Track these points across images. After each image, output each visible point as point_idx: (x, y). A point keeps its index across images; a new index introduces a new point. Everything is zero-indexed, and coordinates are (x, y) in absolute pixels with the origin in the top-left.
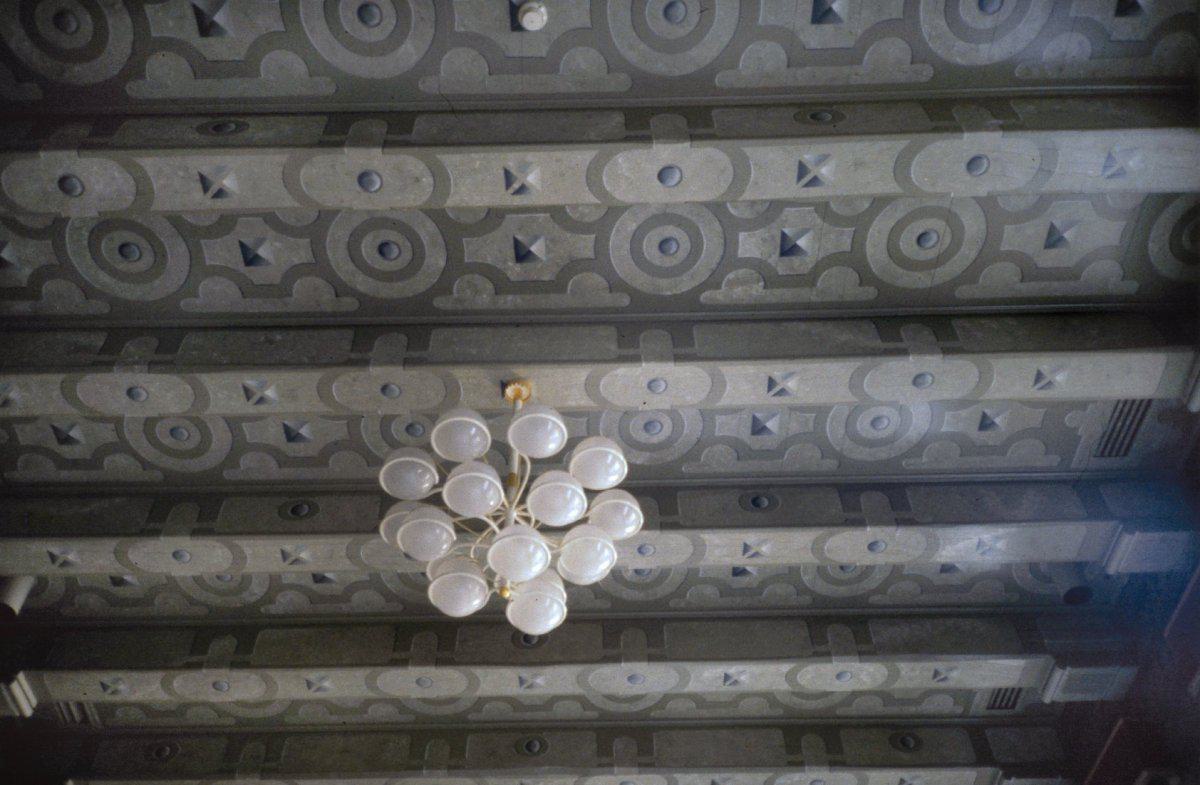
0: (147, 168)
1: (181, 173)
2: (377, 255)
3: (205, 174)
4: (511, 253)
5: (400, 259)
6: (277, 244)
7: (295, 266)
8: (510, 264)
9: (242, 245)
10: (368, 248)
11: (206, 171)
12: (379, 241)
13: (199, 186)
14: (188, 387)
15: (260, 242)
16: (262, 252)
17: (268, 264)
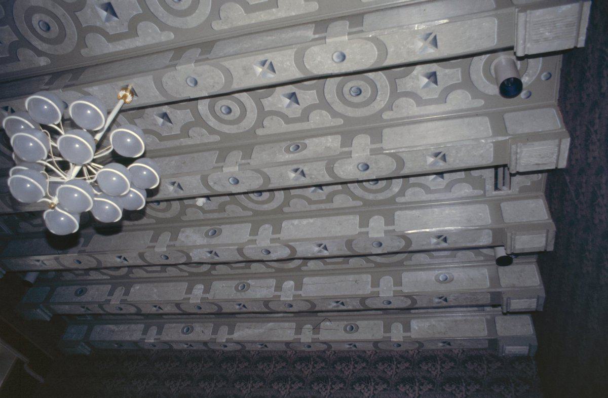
0: (328, 177)
1: (313, 176)
2: (231, 107)
3: (303, 177)
4: (170, 116)
5: (220, 106)
6: (280, 106)
7: (270, 96)
8: (168, 111)
9: (298, 103)
10: (236, 110)
11: (303, 179)
12: (232, 114)
13: (305, 172)
14: (308, 67)
15: (289, 106)
16: (288, 101)
17: (284, 95)
